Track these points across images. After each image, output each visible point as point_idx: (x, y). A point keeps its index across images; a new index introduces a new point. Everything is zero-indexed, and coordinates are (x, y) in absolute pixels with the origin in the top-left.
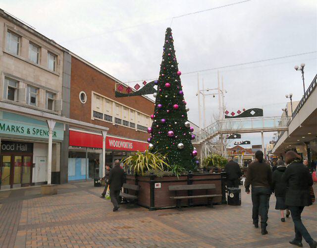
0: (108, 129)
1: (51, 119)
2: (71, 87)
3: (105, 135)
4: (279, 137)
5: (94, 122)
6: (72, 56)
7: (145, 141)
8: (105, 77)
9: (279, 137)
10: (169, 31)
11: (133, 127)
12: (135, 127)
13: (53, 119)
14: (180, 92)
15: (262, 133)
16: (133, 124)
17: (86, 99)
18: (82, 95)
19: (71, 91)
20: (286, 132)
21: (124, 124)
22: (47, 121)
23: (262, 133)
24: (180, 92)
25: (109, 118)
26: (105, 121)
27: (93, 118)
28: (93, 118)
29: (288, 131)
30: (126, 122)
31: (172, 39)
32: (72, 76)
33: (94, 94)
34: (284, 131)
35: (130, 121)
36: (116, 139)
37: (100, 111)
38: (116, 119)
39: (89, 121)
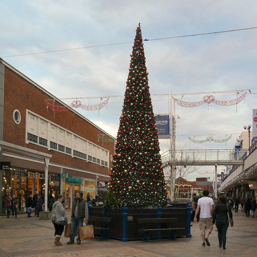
0: (50, 156)
1: (47, 157)
2: (5, 104)
3: (48, 163)
4: (231, 172)
5: (29, 146)
6: (6, 67)
7: (107, 175)
8: (40, 92)
9: (231, 172)
10: (139, 30)
11: (34, 141)
12: (100, 163)
13: (49, 157)
14: (128, 88)
15: (216, 167)
16: (69, 150)
17: (20, 119)
18: (16, 113)
19: (4, 109)
20: (241, 166)
21: (105, 165)
22: (44, 159)
23: (216, 167)
24: (128, 88)
25: (44, 141)
26: (97, 164)
27: (27, 142)
28: (27, 142)
29: (243, 165)
30: (62, 147)
31: (144, 69)
32: (5, 91)
33: (29, 112)
34: (239, 165)
35: (66, 146)
36: (1, 159)
37: (62, 144)
38: (51, 142)
39: (23, 144)
